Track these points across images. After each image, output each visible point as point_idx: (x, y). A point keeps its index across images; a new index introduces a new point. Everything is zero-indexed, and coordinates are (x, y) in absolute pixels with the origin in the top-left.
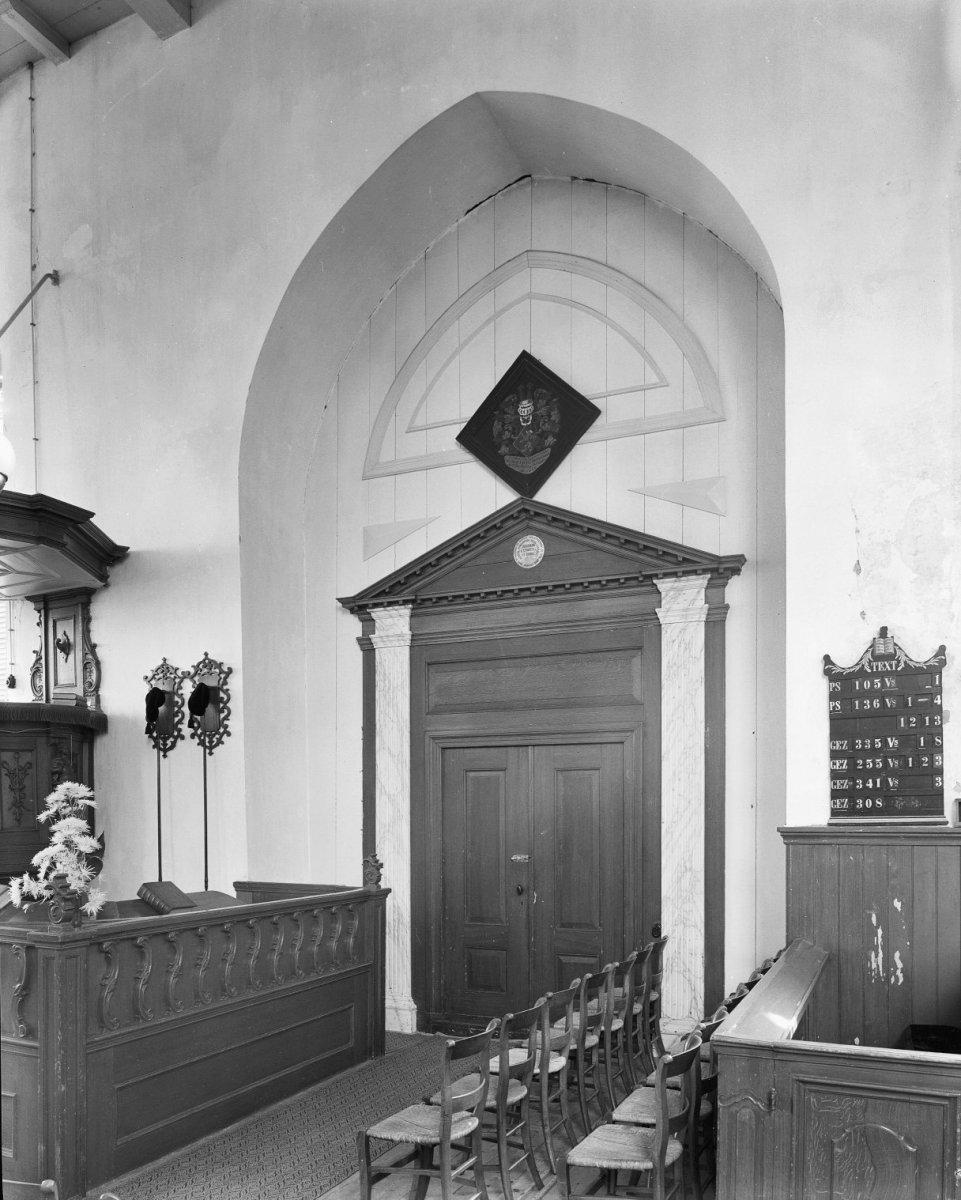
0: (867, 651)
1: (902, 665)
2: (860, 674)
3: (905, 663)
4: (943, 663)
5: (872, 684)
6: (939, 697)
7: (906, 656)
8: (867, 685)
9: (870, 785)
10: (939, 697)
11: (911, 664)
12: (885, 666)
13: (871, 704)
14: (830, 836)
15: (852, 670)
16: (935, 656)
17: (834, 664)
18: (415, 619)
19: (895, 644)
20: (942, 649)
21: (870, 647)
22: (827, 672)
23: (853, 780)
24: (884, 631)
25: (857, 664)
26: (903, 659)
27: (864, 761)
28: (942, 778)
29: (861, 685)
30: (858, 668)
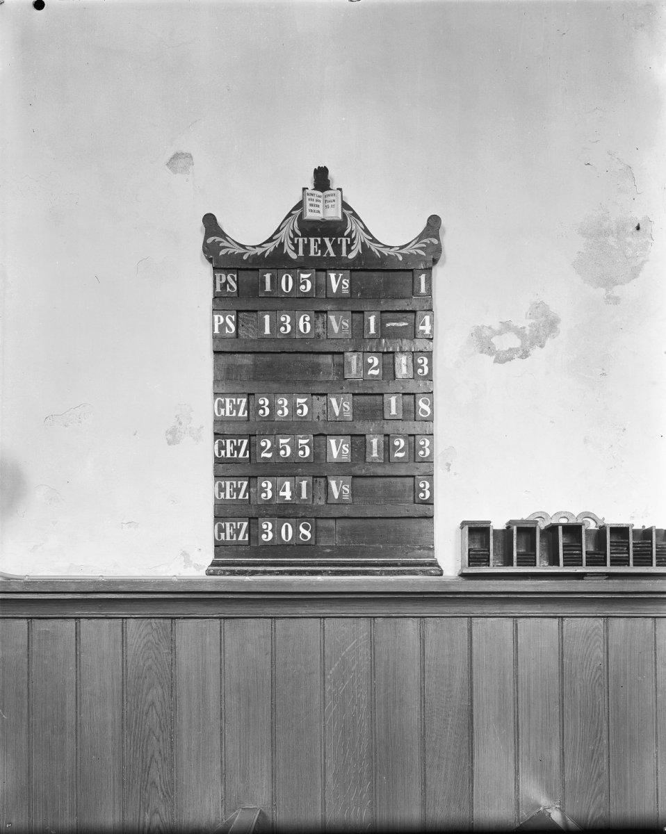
0: (290, 215)
1: (357, 248)
2: (276, 261)
3: (363, 245)
4: (434, 255)
5: (297, 283)
6: (427, 318)
7: (366, 231)
8: (287, 283)
9: (287, 494)
10: (427, 318)
11: (374, 247)
12: (323, 247)
13: (294, 324)
14: (621, 561)
15: (259, 251)
16: (420, 237)
17: (223, 235)
18: (218, 549)
19: (345, 206)
20: (434, 224)
21: (296, 208)
22: (210, 251)
23: (253, 521)
24: (322, 179)
25: (270, 240)
26: (361, 237)
27: (275, 442)
28: (432, 484)
29: (276, 325)
30: (270, 247)
